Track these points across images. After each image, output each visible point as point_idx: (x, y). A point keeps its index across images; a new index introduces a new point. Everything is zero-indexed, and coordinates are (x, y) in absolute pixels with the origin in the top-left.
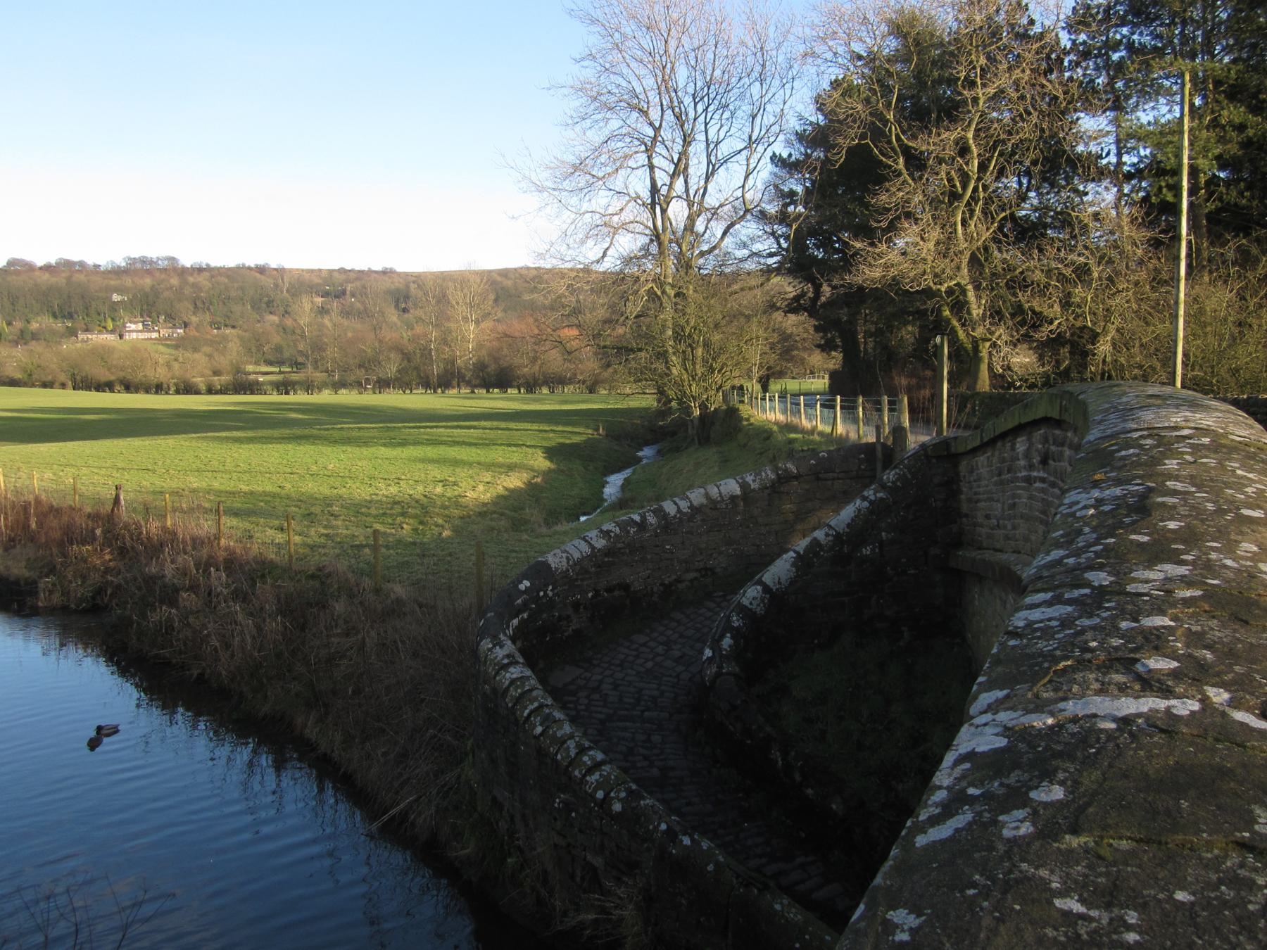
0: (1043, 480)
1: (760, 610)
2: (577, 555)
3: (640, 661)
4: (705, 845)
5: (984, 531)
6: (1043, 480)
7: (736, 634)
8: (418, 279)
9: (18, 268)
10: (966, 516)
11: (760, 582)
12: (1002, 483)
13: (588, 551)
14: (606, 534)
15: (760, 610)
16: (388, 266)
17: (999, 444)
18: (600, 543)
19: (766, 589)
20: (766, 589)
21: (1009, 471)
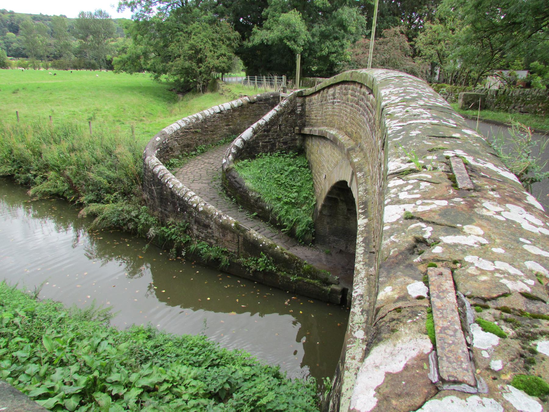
0: (338, 102)
1: (241, 147)
2: (175, 129)
3: (199, 165)
4: (231, 218)
5: (314, 121)
6: (338, 102)
7: (233, 154)
8: (22, 18)
9: (4, 12)
10: (307, 116)
11: (241, 137)
12: (322, 105)
13: (179, 127)
14: (185, 121)
15: (241, 147)
16: (63, 14)
17: (322, 92)
18: (183, 125)
19: (243, 140)
20: (243, 140)
21: (325, 100)
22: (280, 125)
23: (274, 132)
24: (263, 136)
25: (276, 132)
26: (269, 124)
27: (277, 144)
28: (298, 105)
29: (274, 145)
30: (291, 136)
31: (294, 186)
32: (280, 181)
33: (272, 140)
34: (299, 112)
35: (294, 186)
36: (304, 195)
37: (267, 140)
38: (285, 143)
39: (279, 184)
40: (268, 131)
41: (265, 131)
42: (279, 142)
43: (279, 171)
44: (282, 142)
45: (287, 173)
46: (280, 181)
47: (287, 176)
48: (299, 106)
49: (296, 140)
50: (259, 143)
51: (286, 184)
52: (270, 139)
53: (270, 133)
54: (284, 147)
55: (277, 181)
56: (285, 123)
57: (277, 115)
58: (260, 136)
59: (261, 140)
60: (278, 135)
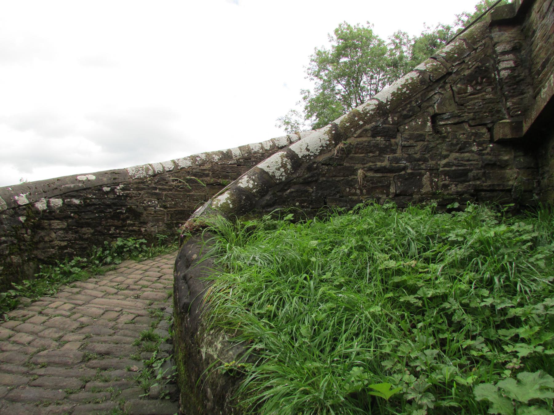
22: (435, 118)
23: (411, 137)
24: (367, 149)
25: (420, 138)
26: (393, 111)
27: (425, 179)
28: (499, 49)
29: (414, 179)
30: (480, 153)
31: (516, 322)
32: (413, 290)
33: (403, 163)
34: (504, 74)
35: (516, 322)
36: (406, 314)
37: (386, 163)
38: (459, 176)
39: (408, 305)
40: (390, 134)
41: (375, 132)
42: (434, 171)
43: (414, 247)
44: (446, 173)
45: (457, 253)
46: (413, 290)
47: (463, 263)
48: (504, 53)
49: (504, 165)
50: (354, 172)
51: (452, 304)
52: (397, 160)
53: (399, 140)
54: (453, 188)
55: (394, 285)
56: (452, 108)
57: (422, 81)
58: (359, 148)
59: (363, 161)
60: (427, 149)
